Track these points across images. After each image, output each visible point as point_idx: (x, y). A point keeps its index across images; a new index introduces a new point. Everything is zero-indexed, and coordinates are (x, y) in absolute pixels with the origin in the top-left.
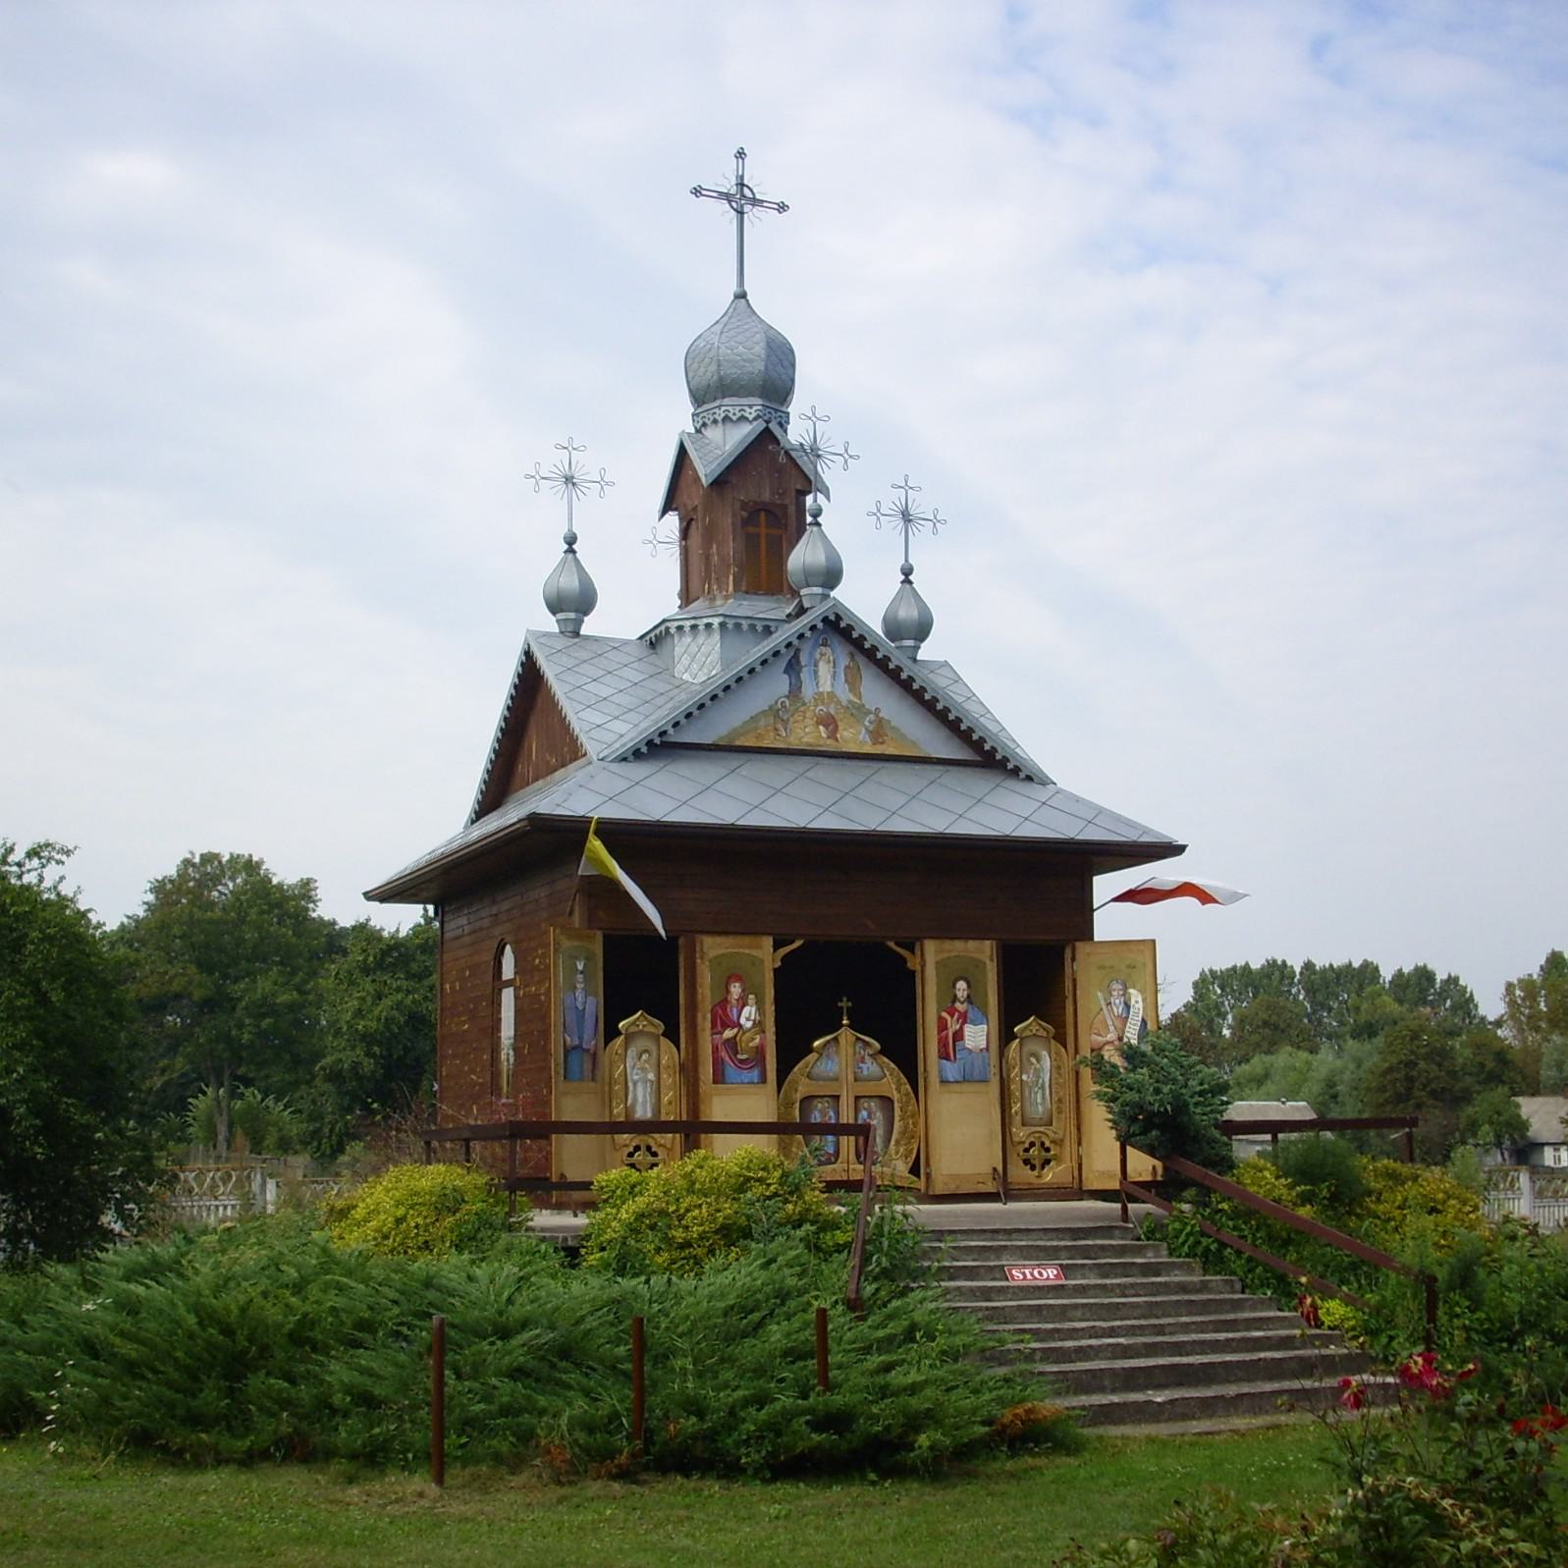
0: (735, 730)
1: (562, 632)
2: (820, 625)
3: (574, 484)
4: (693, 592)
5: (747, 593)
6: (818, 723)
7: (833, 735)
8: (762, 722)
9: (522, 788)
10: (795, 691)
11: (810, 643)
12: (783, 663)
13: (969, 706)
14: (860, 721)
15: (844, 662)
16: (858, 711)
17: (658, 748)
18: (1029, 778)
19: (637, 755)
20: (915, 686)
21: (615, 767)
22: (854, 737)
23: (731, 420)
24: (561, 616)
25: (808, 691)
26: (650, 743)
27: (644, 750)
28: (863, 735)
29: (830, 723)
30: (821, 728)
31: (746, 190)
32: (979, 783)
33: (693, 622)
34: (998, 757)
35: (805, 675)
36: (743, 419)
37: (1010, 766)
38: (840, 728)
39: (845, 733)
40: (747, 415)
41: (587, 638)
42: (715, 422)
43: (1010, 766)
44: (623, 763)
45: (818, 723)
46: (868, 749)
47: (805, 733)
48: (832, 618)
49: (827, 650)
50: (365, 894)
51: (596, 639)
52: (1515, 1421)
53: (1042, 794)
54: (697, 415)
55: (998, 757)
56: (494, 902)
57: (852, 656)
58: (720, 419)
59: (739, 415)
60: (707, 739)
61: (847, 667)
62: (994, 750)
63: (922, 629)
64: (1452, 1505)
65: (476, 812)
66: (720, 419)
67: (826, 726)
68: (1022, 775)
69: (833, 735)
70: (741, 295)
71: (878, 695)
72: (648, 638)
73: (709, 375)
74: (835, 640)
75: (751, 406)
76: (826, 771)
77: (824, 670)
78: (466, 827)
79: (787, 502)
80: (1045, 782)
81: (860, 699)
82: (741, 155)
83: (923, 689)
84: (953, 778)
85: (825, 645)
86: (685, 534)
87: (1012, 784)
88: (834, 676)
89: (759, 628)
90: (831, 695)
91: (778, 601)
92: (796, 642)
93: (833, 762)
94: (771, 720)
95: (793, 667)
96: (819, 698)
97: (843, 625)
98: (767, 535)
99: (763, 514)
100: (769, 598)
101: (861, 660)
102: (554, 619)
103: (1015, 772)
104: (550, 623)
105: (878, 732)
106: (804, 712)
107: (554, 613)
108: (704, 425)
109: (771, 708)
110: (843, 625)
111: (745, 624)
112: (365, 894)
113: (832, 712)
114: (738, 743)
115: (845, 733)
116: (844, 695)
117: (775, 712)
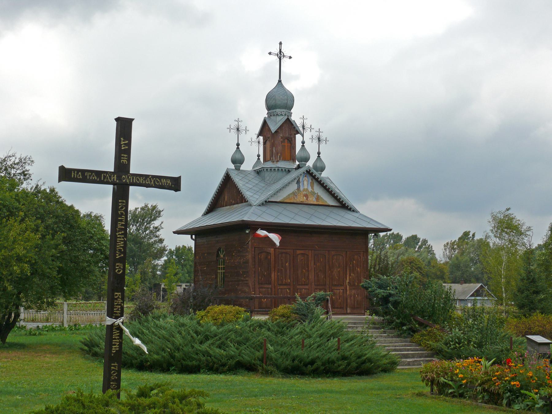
0: (284, 198)
1: (235, 169)
2: (305, 172)
3: (239, 131)
4: (267, 159)
5: (282, 160)
6: (304, 196)
7: (307, 199)
8: (291, 196)
9: (221, 207)
10: (299, 188)
11: (302, 176)
12: (296, 181)
13: (332, 185)
14: (313, 196)
15: (310, 181)
16: (313, 193)
17: (267, 203)
18: (353, 211)
19: (263, 204)
20: (322, 182)
21: (259, 208)
22: (312, 200)
23: (278, 115)
24: (235, 165)
25: (301, 189)
26: (266, 202)
27: (264, 203)
28: (314, 199)
29: (306, 196)
30: (304, 197)
31: (282, 53)
32: (342, 212)
33: (270, 168)
34: (346, 205)
35: (301, 184)
36: (282, 115)
37: (349, 208)
38: (309, 197)
39: (310, 199)
40: (282, 114)
41: (242, 170)
42: (274, 115)
43: (349, 208)
44: (260, 207)
45: (304, 196)
46: (315, 203)
47: (302, 199)
48: (308, 170)
49: (306, 178)
50: (173, 232)
51: (244, 171)
52: (398, 255)
53: (356, 215)
54: (269, 113)
55: (346, 205)
56: (217, 237)
57: (312, 179)
58: (275, 115)
59: (280, 114)
60: (278, 200)
61: (311, 182)
62: (345, 204)
63: (322, 169)
64: (414, 255)
65: (206, 212)
66: (275, 115)
67: (306, 197)
68: (352, 210)
69: (307, 199)
70: (280, 81)
71: (318, 190)
72: (257, 171)
73: (273, 103)
74: (308, 175)
75: (283, 112)
76: (305, 208)
77: (305, 183)
78: (202, 216)
79: (292, 137)
80: (357, 212)
81: (314, 190)
82: (281, 43)
83: (329, 188)
84: (336, 210)
85: (306, 177)
86: (265, 143)
87: (349, 212)
88: (308, 184)
89: (287, 171)
90: (307, 189)
91: (289, 162)
92: (299, 176)
93: (307, 206)
94: (293, 195)
95: (298, 182)
96: (304, 190)
97: (311, 172)
98: (285, 143)
99: (286, 140)
100: (288, 162)
101: (314, 180)
102: (234, 165)
103: (350, 209)
104: (232, 166)
105: (318, 198)
106: (301, 193)
107: (234, 164)
108: (271, 115)
109: (293, 192)
110: (311, 172)
111: (280, 169)
112: (173, 232)
113: (307, 193)
114: (285, 201)
115: (310, 199)
116: (310, 189)
117: (294, 193)
